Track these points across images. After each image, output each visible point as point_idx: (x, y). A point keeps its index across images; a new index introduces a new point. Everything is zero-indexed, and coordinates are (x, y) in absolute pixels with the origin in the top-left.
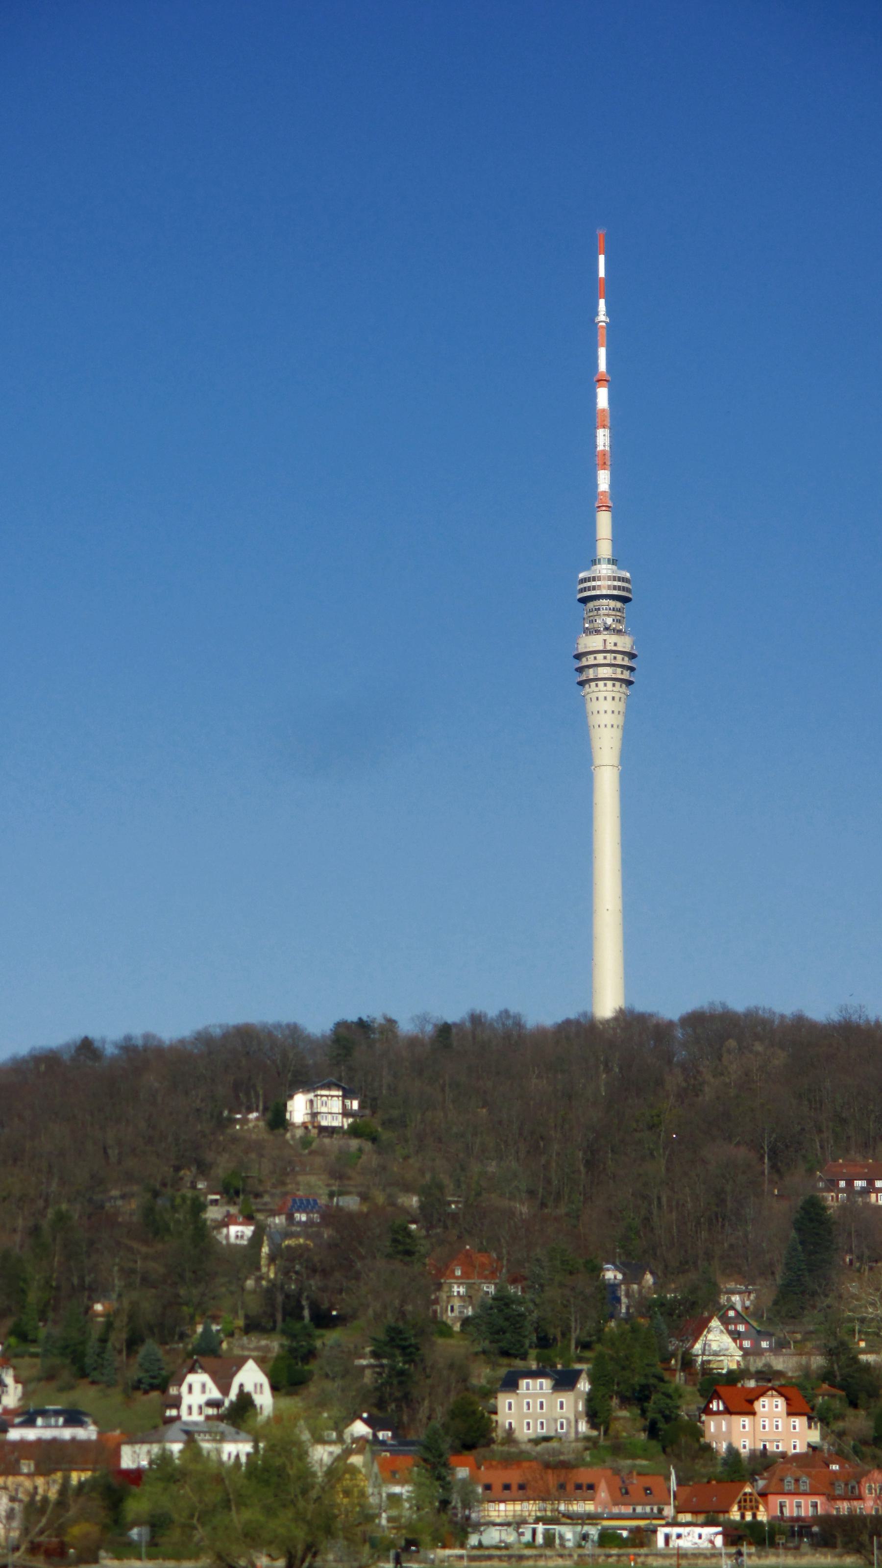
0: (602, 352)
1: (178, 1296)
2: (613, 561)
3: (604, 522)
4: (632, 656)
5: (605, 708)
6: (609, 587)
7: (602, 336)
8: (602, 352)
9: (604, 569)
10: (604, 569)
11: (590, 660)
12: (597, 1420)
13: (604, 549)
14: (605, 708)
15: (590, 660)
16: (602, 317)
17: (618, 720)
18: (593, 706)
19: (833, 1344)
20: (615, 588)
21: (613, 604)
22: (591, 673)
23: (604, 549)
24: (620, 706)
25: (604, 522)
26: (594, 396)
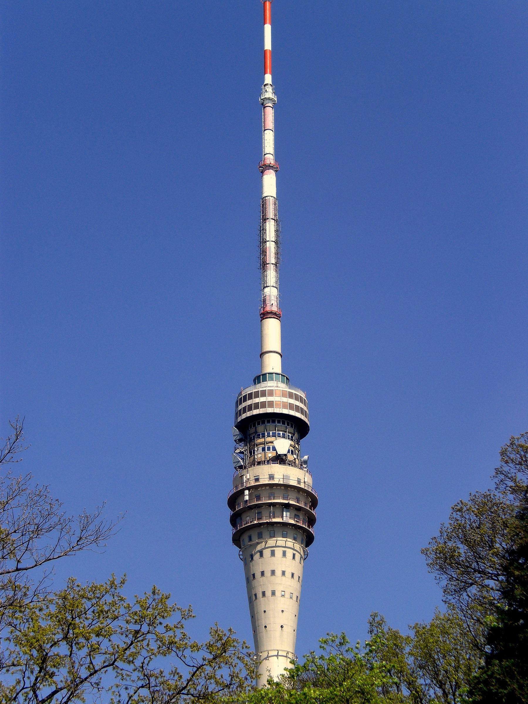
6: (285, 405)
13: (273, 364)
20: (291, 406)
23: (273, 364)
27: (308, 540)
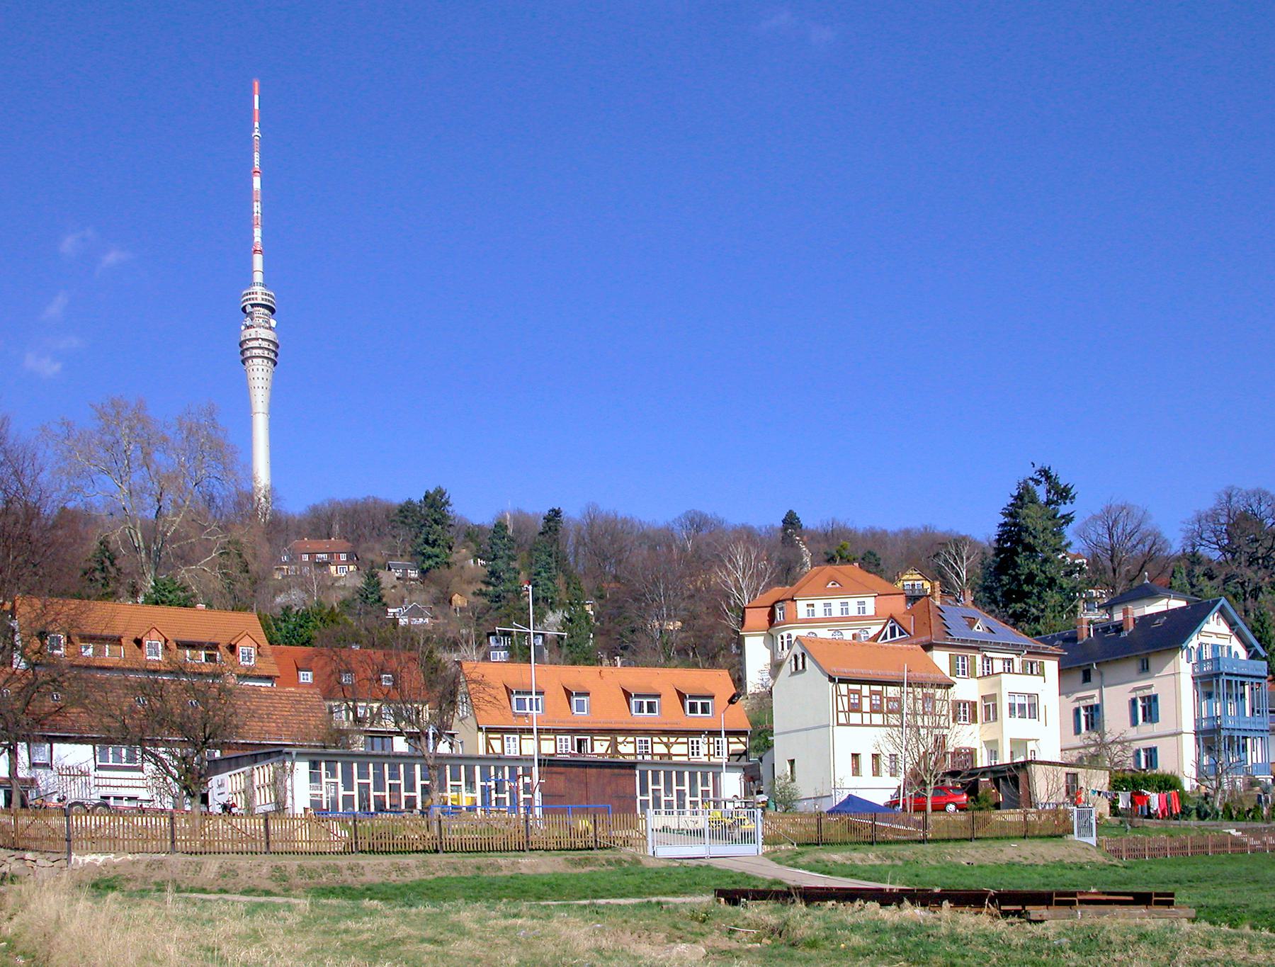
0: (257, 106)
1: (899, 937)
2: (264, 285)
3: (258, 260)
4: (277, 346)
5: (259, 374)
7: (257, 145)
8: (256, 155)
9: (258, 289)
10: (258, 289)
11: (251, 344)
12: (890, 574)
13: (258, 277)
14: (259, 374)
15: (251, 344)
16: (258, 233)
17: (267, 384)
18: (251, 375)
19: (234, 810)
21: (262, 310)
22: (248, 354)
23: (258, 277)
24: (269, 376)
25: (258, 260)
26: (252, 182)
27: (275, 364)
